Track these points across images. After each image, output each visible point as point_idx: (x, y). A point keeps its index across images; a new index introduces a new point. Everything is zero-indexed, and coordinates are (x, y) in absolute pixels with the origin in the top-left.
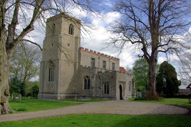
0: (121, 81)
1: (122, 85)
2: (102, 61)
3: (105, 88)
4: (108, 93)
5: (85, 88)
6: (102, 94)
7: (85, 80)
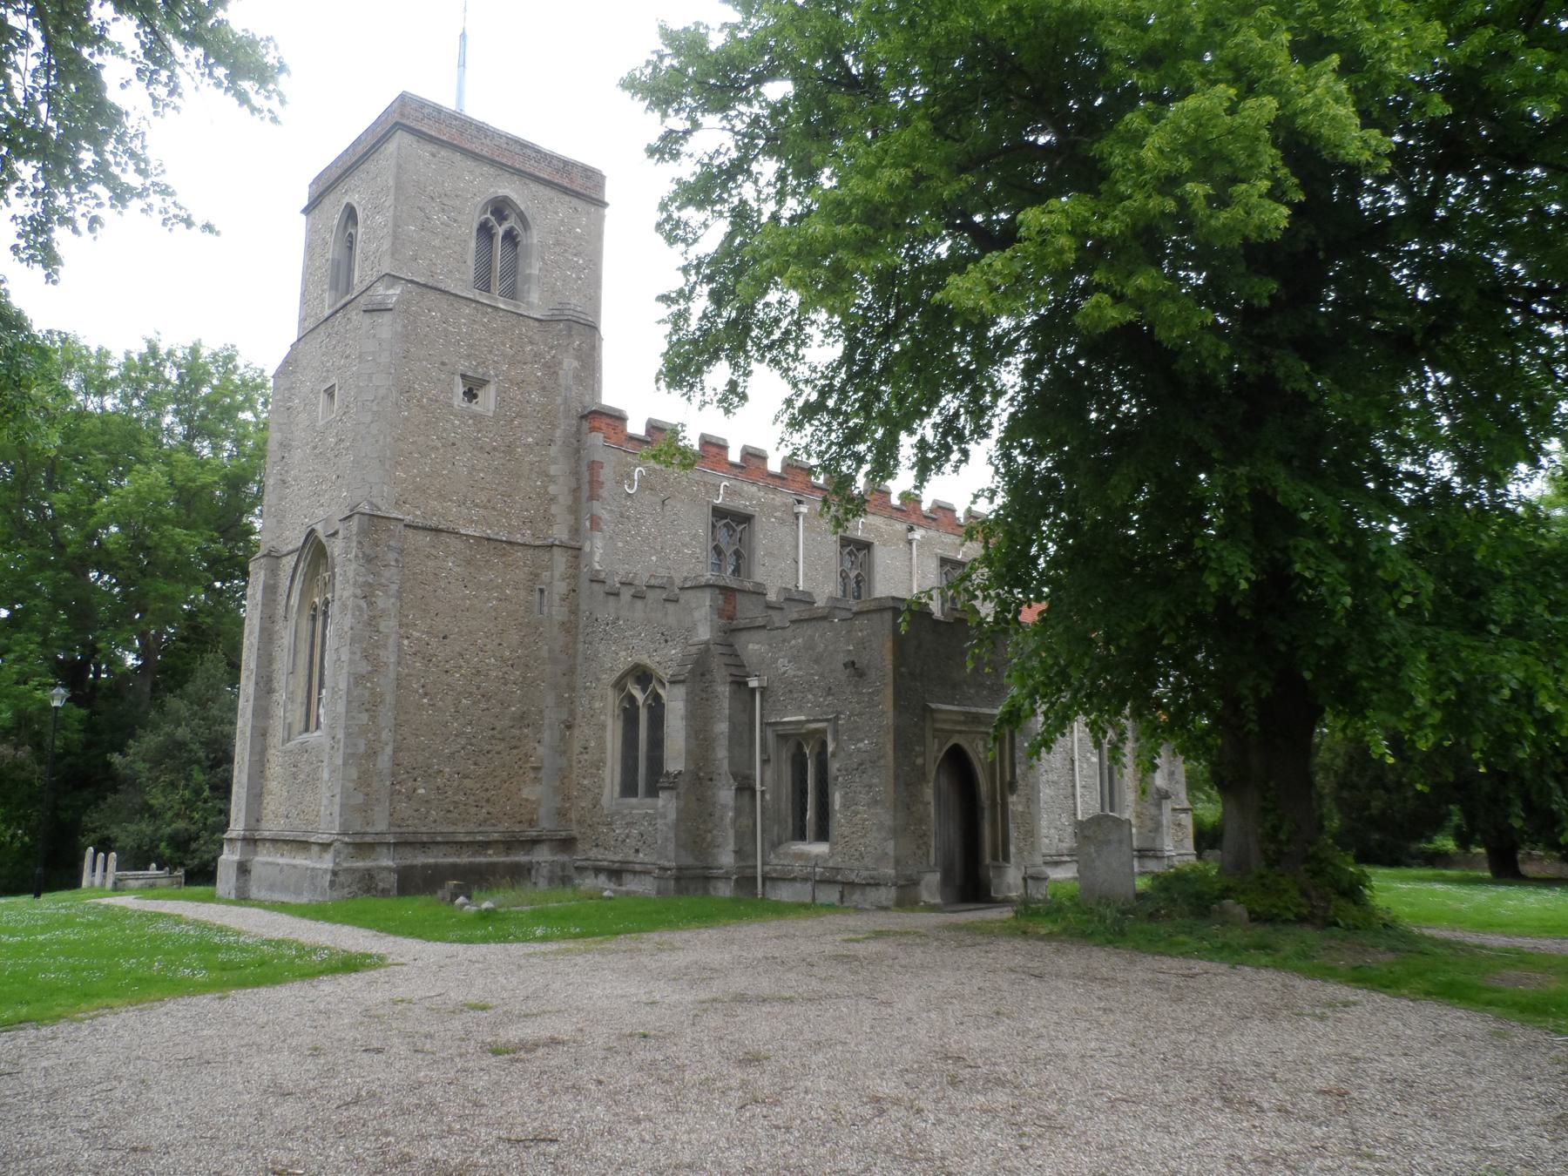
5: (629, 789)
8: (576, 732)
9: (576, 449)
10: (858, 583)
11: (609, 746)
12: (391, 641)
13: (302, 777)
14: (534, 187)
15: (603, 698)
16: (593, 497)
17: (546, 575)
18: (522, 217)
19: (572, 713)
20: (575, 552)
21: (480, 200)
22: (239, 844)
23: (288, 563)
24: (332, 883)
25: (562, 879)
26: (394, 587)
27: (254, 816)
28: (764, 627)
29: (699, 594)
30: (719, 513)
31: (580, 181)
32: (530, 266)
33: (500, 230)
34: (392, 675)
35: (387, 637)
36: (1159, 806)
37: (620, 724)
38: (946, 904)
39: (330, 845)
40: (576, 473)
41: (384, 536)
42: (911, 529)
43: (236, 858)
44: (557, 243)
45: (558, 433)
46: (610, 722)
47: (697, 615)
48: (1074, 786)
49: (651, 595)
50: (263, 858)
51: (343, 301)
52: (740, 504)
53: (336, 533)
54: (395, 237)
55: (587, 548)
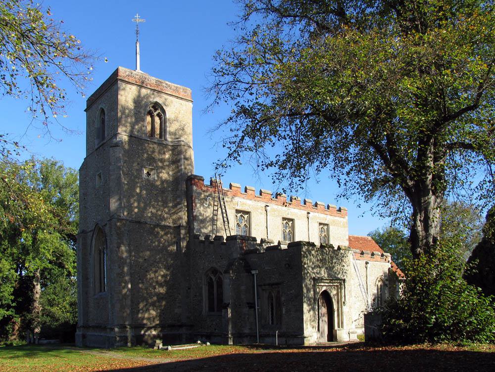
13: (101, 307)
23: (90, 234)
31: (182, 93)
43: (81, 333)
51: (102, 143)
53: (106, 224)
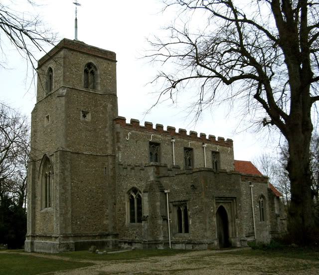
0: (221, 195)
1: (226, 207)
2: (182, 148)
3: (132, 208)
4: (187, 231)
5: (132, 220)
6: (173, 235)
7: (178, 211)
8: (117, 205)
9: (113, 129)
10: (189, 160)
11: (126, 209)
12: (69, 184)
14: (98, 59)
15: (124, 196)
16: (118, 141)
17: (106, 164)
18: (95, 67)
19: (116, 201)
20: (114, 157)
21: (84, 64)
22: (30, 237)
24: (59, 247)
25: (116, 246)
26: (69, 169)
27: (34, 231)
28: (168, 176)
29: (150, 168)
30: (151, 143)
32: (98, 80)
33: (90, 69)
34: (70, 193)
35: (68, 182)
36: (276, 219)
37: (129, 203)
38: (220, 248)
39: (58, 237)
40: (113, 135)
41: (66, 156)
42: (204, 144)
43: (30, 241)
44: (104, 73)
45: (108, 125)
46: (126, 202)
47: (149, 174)
48: (253, 215)
49: (136, 168)
50: (37, 241)
52: (157, 140)
54: (64, 76)
55: (117, 156)
